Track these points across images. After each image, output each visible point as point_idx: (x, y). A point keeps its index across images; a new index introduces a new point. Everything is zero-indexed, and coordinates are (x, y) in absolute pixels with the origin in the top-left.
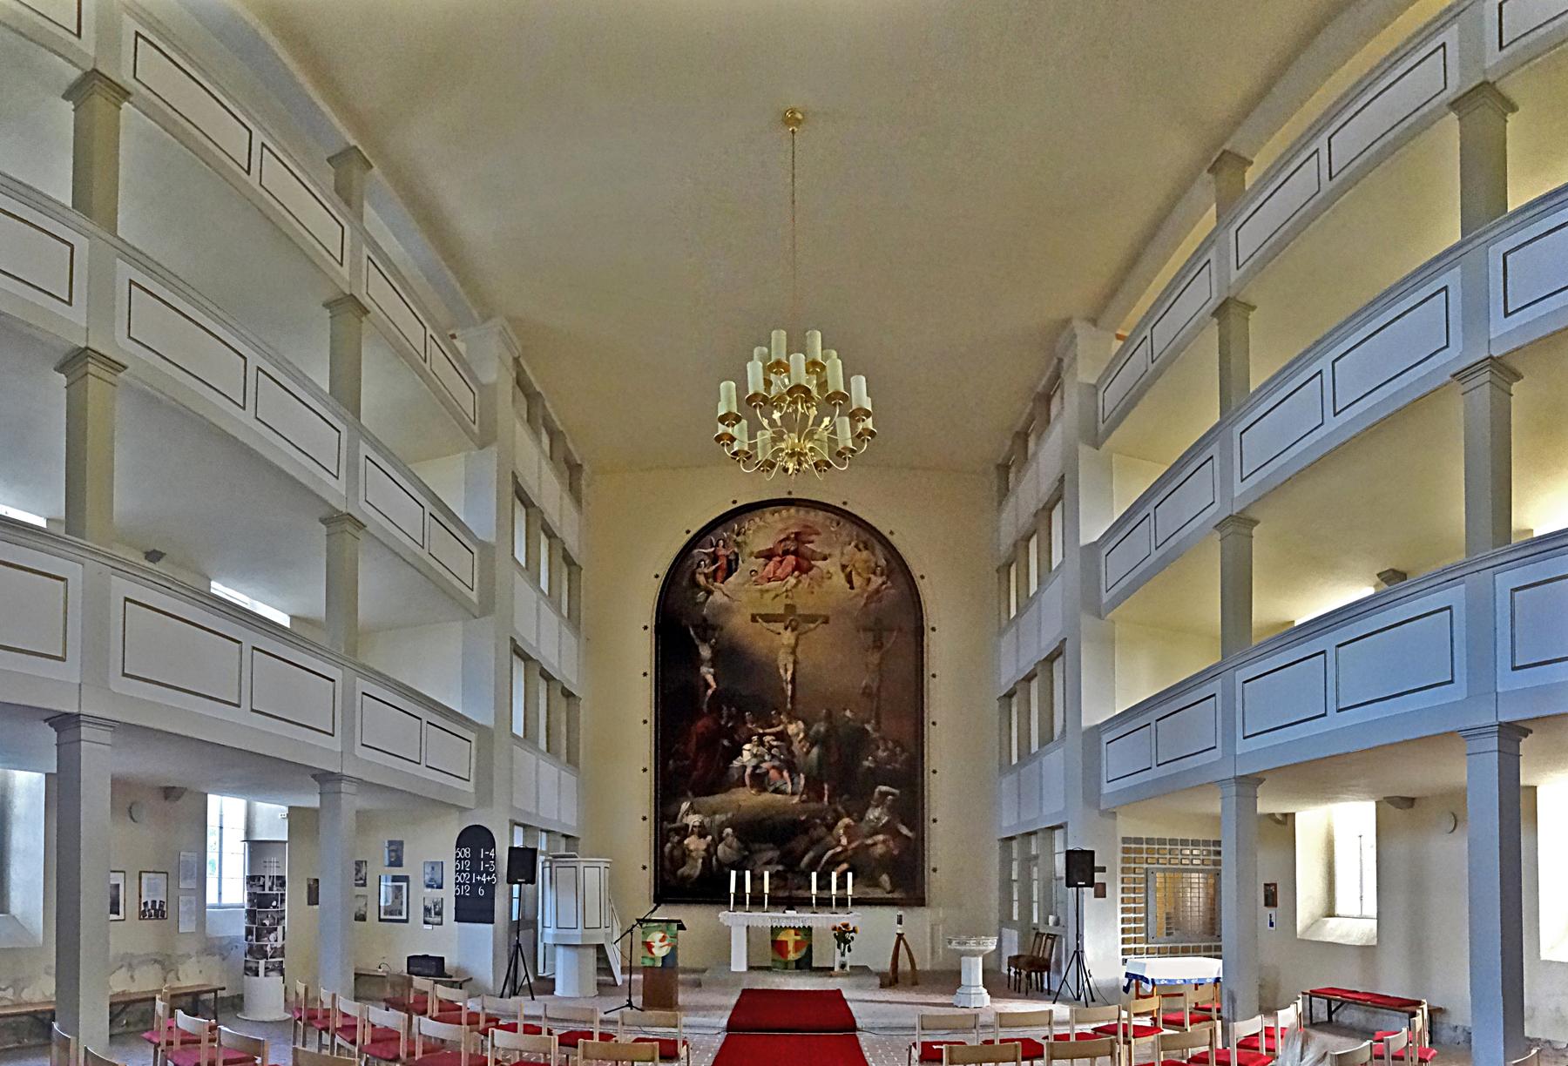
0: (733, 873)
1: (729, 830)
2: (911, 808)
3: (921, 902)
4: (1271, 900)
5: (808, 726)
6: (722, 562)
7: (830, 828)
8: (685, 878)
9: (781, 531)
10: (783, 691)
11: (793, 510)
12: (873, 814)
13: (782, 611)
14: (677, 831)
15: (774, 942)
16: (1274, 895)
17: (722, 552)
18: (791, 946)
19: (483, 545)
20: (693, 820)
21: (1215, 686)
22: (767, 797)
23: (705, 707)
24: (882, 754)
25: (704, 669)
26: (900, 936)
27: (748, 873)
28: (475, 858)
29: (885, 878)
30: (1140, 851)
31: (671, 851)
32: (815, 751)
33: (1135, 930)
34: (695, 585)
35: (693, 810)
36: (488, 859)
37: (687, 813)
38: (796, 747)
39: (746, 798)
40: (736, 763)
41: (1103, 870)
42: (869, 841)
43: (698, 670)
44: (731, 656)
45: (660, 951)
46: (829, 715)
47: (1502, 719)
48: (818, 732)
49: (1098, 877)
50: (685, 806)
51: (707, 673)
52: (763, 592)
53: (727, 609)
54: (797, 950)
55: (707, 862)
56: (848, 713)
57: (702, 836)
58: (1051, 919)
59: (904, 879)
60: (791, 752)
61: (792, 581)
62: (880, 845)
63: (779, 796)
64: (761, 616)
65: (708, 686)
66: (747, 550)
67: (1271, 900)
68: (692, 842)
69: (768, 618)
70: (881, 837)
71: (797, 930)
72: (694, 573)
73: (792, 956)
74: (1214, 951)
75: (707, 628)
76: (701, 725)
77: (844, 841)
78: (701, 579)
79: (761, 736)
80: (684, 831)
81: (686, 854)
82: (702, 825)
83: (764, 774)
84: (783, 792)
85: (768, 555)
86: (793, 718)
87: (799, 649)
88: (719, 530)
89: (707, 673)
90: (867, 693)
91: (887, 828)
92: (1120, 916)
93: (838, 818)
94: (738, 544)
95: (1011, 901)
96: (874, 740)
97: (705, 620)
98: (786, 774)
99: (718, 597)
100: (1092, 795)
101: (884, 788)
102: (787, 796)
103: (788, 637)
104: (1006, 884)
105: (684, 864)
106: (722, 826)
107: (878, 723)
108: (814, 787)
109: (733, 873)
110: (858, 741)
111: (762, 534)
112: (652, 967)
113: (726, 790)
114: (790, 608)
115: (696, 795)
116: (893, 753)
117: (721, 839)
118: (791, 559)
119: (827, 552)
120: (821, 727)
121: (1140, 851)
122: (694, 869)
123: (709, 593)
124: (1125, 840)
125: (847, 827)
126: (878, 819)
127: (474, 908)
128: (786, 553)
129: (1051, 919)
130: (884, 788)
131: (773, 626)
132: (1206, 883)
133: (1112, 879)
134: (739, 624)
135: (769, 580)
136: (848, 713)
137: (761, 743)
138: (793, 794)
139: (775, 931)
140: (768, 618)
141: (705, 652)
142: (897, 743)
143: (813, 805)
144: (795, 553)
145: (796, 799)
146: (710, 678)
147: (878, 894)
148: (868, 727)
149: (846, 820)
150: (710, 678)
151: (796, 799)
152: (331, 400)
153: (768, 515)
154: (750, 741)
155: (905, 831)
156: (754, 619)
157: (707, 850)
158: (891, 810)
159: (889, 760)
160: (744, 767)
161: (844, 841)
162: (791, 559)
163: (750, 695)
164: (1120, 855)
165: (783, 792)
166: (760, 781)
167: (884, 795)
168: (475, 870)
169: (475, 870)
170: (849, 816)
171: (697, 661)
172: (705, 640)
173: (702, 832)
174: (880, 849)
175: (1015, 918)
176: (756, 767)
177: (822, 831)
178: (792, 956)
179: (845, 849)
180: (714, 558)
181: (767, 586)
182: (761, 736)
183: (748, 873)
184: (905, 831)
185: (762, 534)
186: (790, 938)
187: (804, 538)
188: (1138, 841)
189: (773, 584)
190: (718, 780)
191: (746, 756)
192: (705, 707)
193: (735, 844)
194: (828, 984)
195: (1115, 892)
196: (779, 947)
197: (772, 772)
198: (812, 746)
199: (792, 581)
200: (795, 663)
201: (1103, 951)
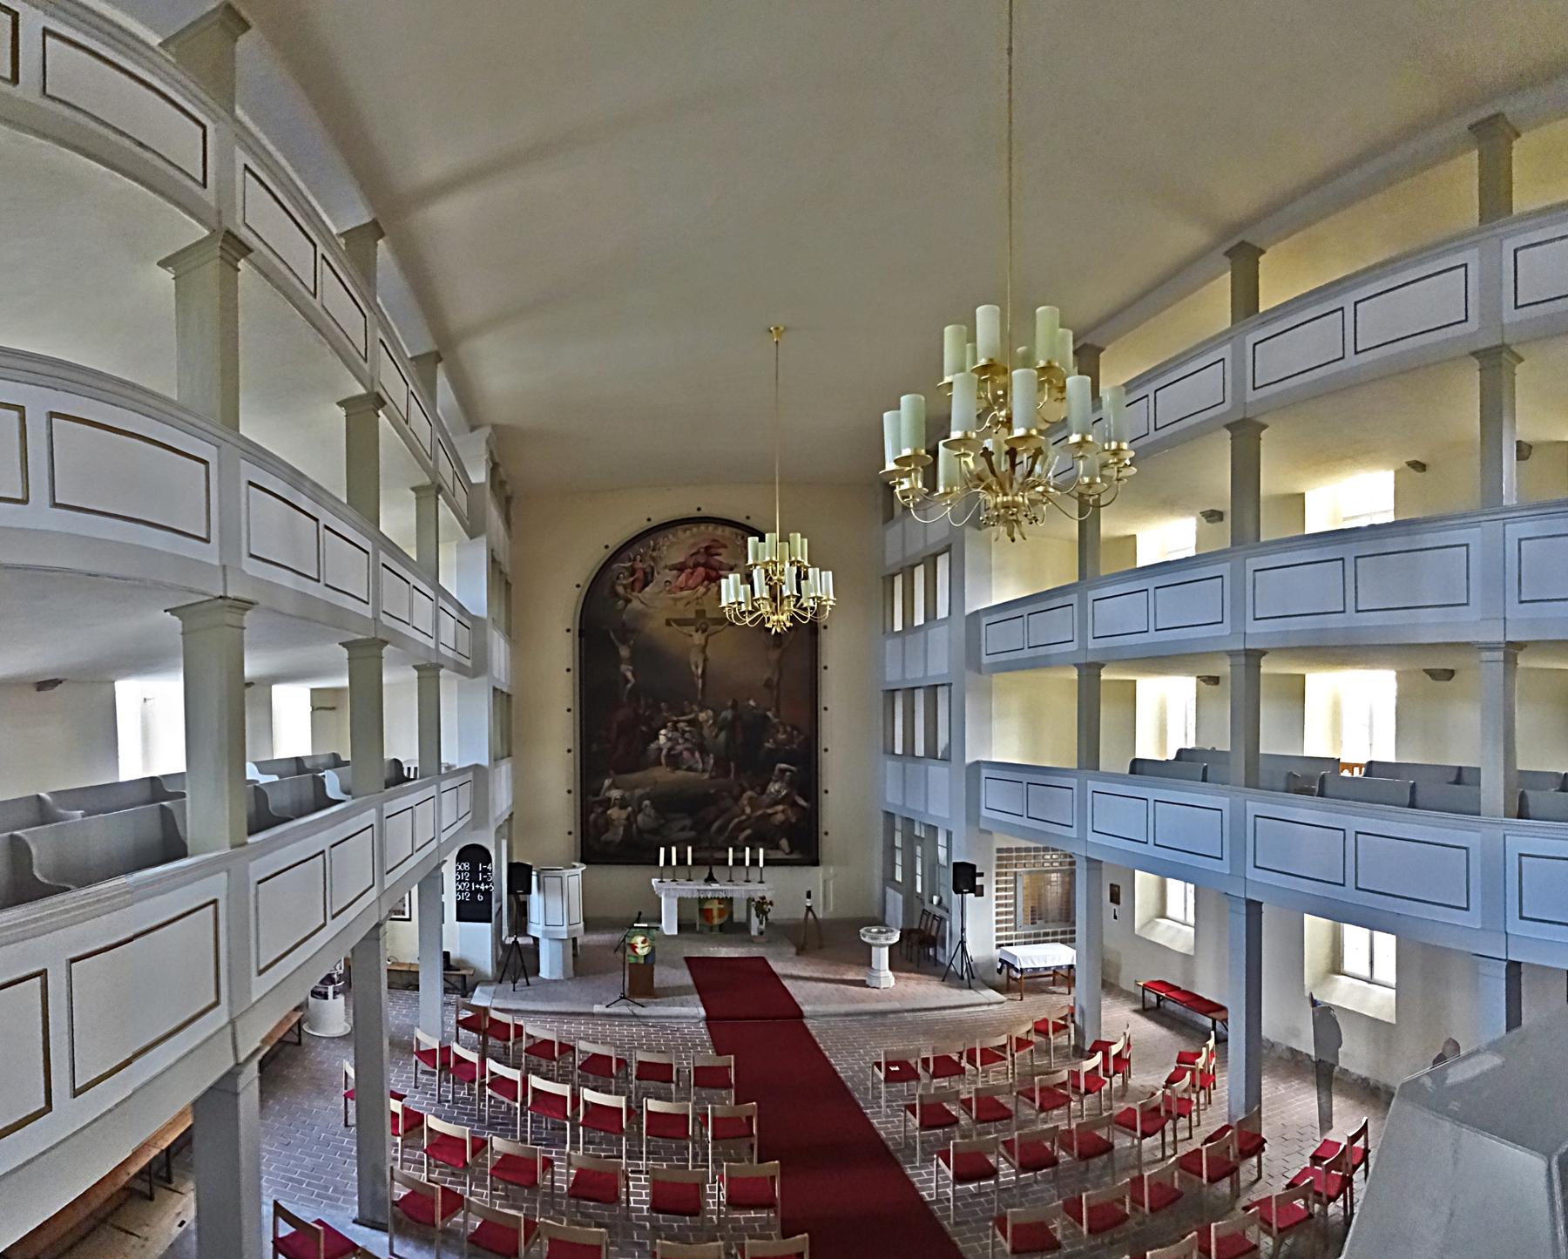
0: (662, 850)
1: (647, 802)
2: (807, 783)
3: (816, 863)
4: (1115, 898)
5: (716, 714)
6: (639, 574)
7: (737, 799)
8: (607, 843)
9: (693, 545)
10: (695, 685)
11: (703, 527)
12: (773, 787)
13: (693, 616)
14: (600, 803)
15: (701, 910)
16: (1118, 895)
17: (639, 565)
18: (715, 913)
19: (473, 618)
20: (615, 794)
21: (1073, 598)
22: (680, 773)
23: (625, 699)
24: (782, 737)
25: (623, 667)
26: (809, 909)
27: (674, 849)
28: (474, 871)
29: (784, 843)
30: (1010, 858)
31: (595, 821)
32: (722, 736)
33: (1006, 921)
34: (616, 595)
35: (614, 786)
36: (485, 871)
37: (609, 788)
38: (706, 732)
39: (662, 774)
40: (653, 746)
41: (981, 875)
42: (770, 811)
43: (618, 668)
44: (649, 655)
45: (642, 950)
46: (734, 706)
47: (1249, 896)
48: (725, 719)
49: (979, 881)
50: (607, 782)
51: (627, 671)
52: (676, 600)
53: (643, 615)
54: (720, 916)
55: (627, 828)
56: (752, 703)
57: (623, 807)
58: (935, 899)
59: (801, 842)
60: (701, 735)
61: (702, 589)
62: (779, 814)
63: (692, 774)
64: (675, 621)
65: (627, 681)
66: (663, 564)
67: (1115, 898)
68: (614, 812)
69: (682, 622)
70: (780, 808)
71: (721, 900)
72: (613, 586)
73: (716, 921)
74: (1069, 942)
75: (626, 632)
76: (621, 715)
77: (748, 810)
78: (620, 590)
79: (675, 723)
80: (608, 803)
81: (609, 823)
82: (623, 798)
83: (676, 755)
84: (695, 770)
85: (680, 568)
86: (703, 709)
87: (708, 651)
88: (636, 546)
89: (627, 671)
90: (768, 684)
91: (788, 800)
92: (995, 910)
93: (743, 791)
94: (653, 559)
95: (894, 864)
96: (774, 726)
97: (624, 624)
98: (697, 755)
99: (636, 604)
100: (973, 815)
101: (784, 766)
102: (698, 773)
103: (698, 638)
104: (890, 849)
105: (607, 831)
106: (642, 798)
107: (778, 710)
108: (721, 766)
109: (662, 850)
110: (761, 725)
111: (676, 549)
112: (637, 964)
113: (645, 768)
114: (701, 613)
115: (618, 772)
116: (791, 735)
117: (640, 810)
118: (701, 570)
119: (732, 563)
120: (727, 714)
121: (1010, 858)
122: (616, 834)
123: (628, 601)
124: (999, 850)
125: (750, 798)
126: (779, 792)
127: (471, 910)
128: (696, 565)
129: (935, 899)
130: (784, 766)
131: (686, 629)
132: (1063, 882)
133: (988, 882)
134: (655, 626)
135: (682, 589)
136: (752, 703)
137: (675, 729)
138: (704, 771)
139: (701, 901)
140: (682, 622)
141: (624, 652)
142: (794, 728)
143: (722, 780)
144: (705, 565)
145: (706, 776)
146: (629, 675)
147: (779, 855)
148: (769, 714)
149: (749, 793)
150: (629, 675)
151: (706, 776)
152: (352, 514)
153: (680, 533)
154: (665, 727)
155: (802, 802)
156: (668, 623)
157: (628, 818)
158: (790, 784)
159: (790, 740)
160: (660, 749)
161: (748, 810)
162: (701, 570)
163: (668, 687)
164: (995, 862)
165: (695, 770)
166: (674, 761)
167: (783, 771)
168: (474, 879)
169: (474, 879)
170: (752, 789)
171: (619, 660)
172: (624, 641)
173: (623, 804)
174: (780, 817)
175: (899, 878)
176: (670, 750)
177: (728, 802)
178: (716, 921)
179: (749, 817)
180: (633, 571)
181: (680, 594)
182: (675, 723)
183: (674, 849)
184: (802, 802)
185: (676, 549)
186: (715, 907)
187: (713, 551)
188: (1009, 850)
189: (685, 593)
190: (638, 759)
191: (662, 739)
192: (625, 699)
193: (653, 813)
194: (755, 951)
195: (990, 890)
196: (706, 914)
197: (686, 754)
198: (721, 730)
199: (702, 589)
200: (705, 660)
201: (980, 927)
